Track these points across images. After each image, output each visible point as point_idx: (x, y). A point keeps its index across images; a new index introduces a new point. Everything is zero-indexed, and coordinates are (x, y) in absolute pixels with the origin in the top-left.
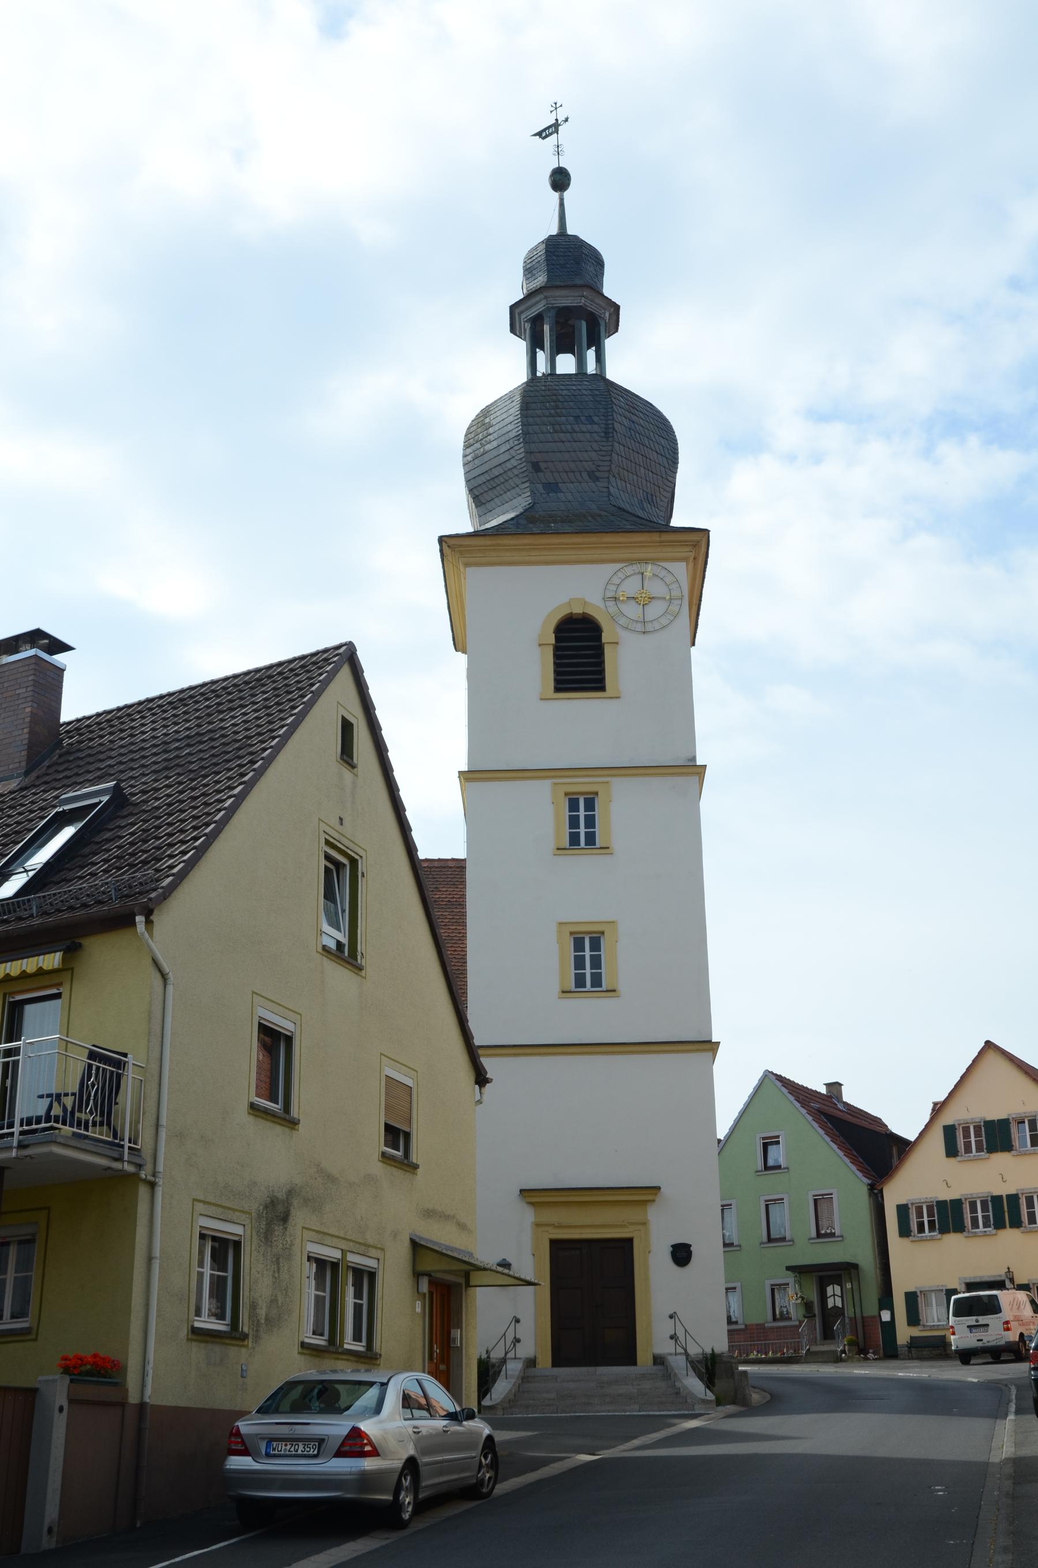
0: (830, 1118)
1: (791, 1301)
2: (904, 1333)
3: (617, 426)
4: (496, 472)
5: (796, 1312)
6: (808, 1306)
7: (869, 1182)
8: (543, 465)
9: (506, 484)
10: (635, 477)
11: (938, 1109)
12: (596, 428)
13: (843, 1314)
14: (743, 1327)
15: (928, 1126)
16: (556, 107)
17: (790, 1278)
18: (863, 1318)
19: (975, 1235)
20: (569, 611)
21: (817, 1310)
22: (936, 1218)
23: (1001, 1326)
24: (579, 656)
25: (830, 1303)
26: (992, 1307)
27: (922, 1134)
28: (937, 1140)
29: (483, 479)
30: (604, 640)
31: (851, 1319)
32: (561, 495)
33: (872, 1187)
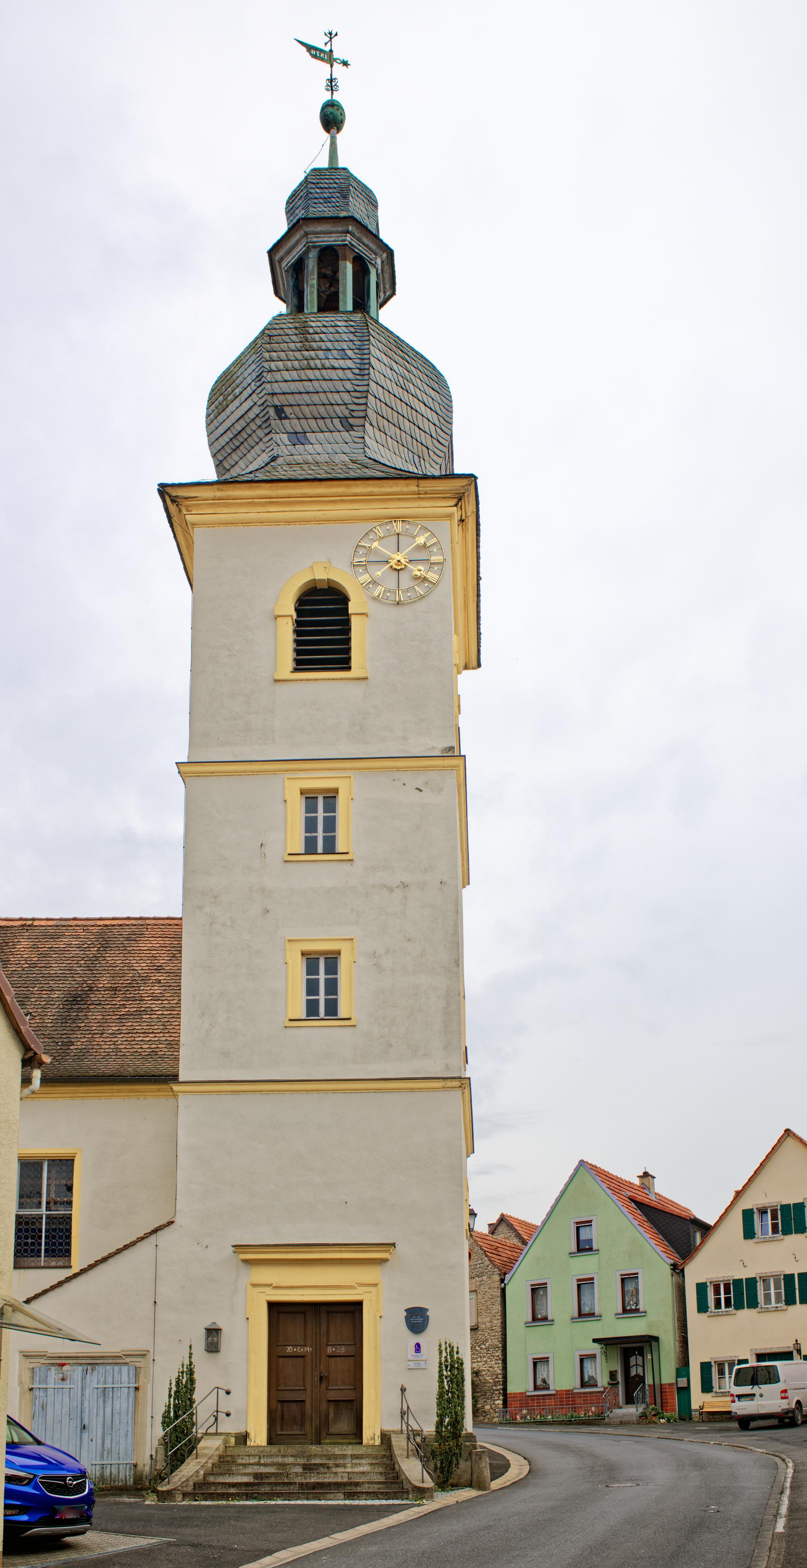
0: (640, 1205)
1: (600, 1372)
2: (698, 1399)
3: (374, 362)
4: (238, 427)
5: (603, 1380)
6: (613, 1375)
7: (672, 1262)
8: (288, 410)
9: (250, 440)
10: (398, 431)
11: (738, 1194)
12: (349, 363)
13: (644, 1382)
14: (554, 1392)
15: (727, 1211)
16: (345, 64)
17: (596, 1348)
18: (661, 1385)
19: (767, 1311)
20: (310, 578)
21: (620, 1378)
22: (732, 1295)
23: (779, 1395)
24: (323, 628)
25: (633, 1373)
26: (771, 1377)
27: (721, 1218)
28: (736, 1221)
29: (226, 438)
30: (350, 612)
31: (649, 1386)
32: (309, 447)
33: (674, 1267)
